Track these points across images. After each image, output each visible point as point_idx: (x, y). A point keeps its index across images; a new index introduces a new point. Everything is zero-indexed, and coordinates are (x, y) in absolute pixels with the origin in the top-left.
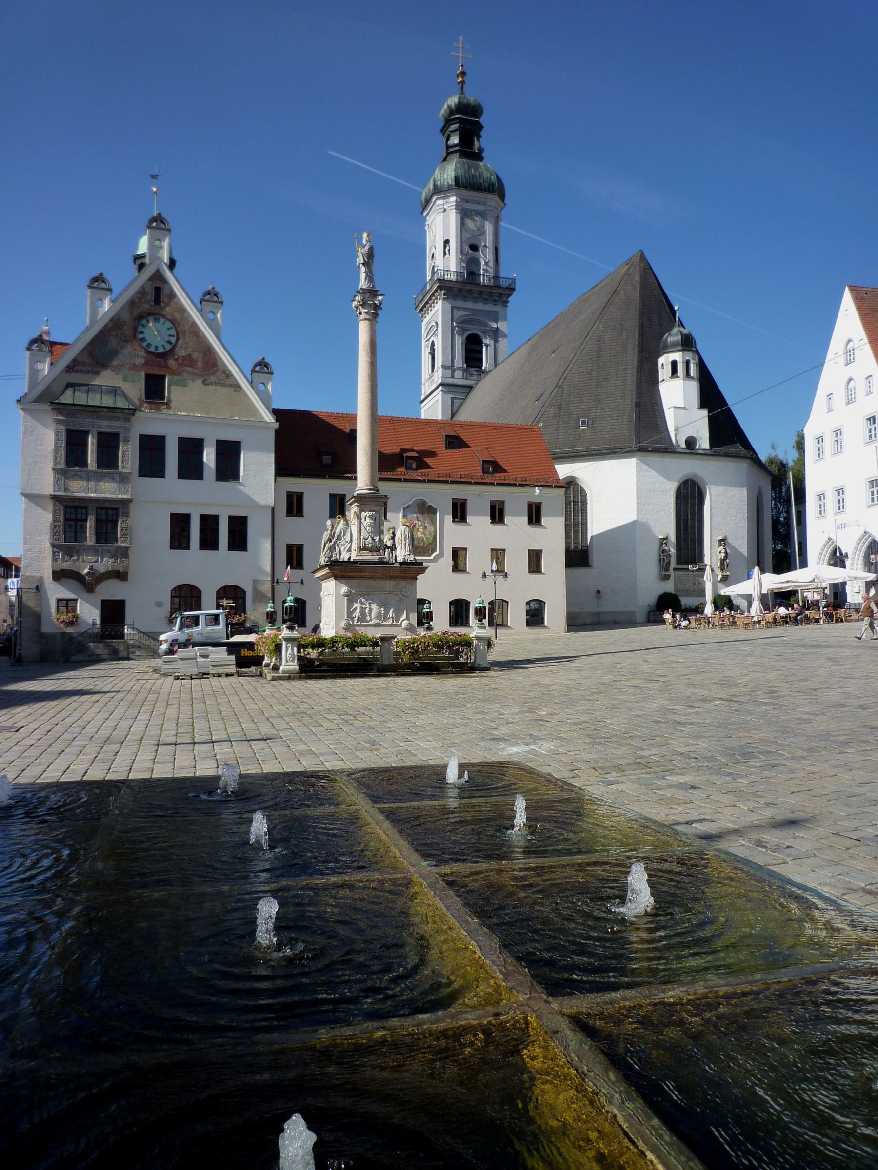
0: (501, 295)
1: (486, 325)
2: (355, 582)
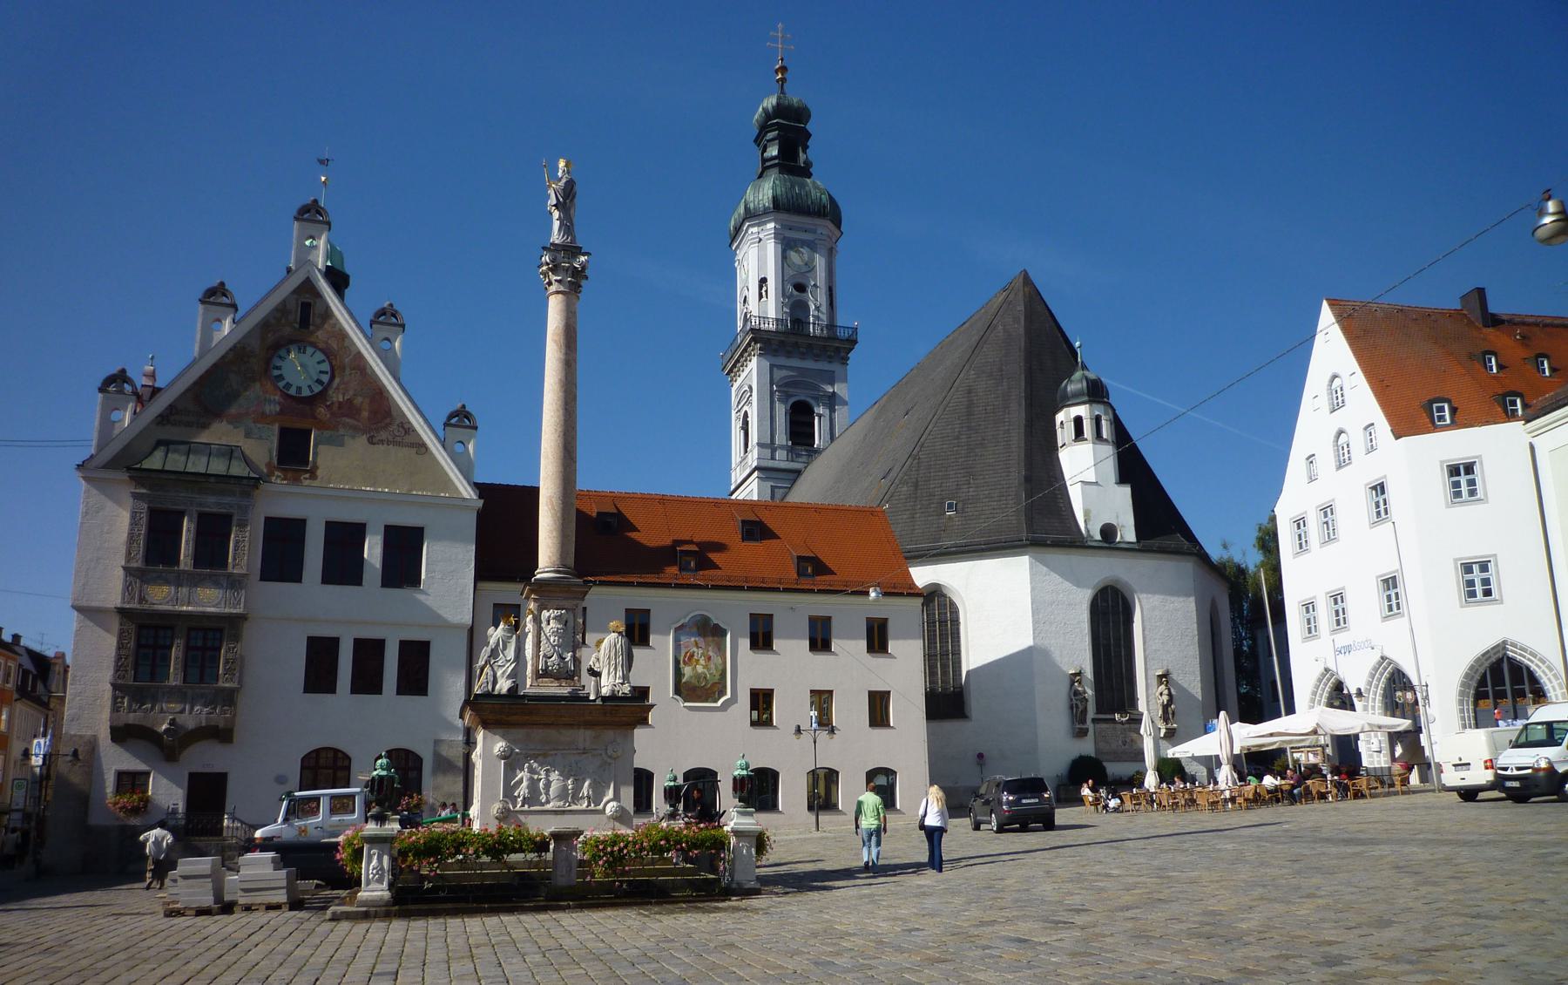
0: (838, 349)
1: (817, 388)
2: (520, 733)
